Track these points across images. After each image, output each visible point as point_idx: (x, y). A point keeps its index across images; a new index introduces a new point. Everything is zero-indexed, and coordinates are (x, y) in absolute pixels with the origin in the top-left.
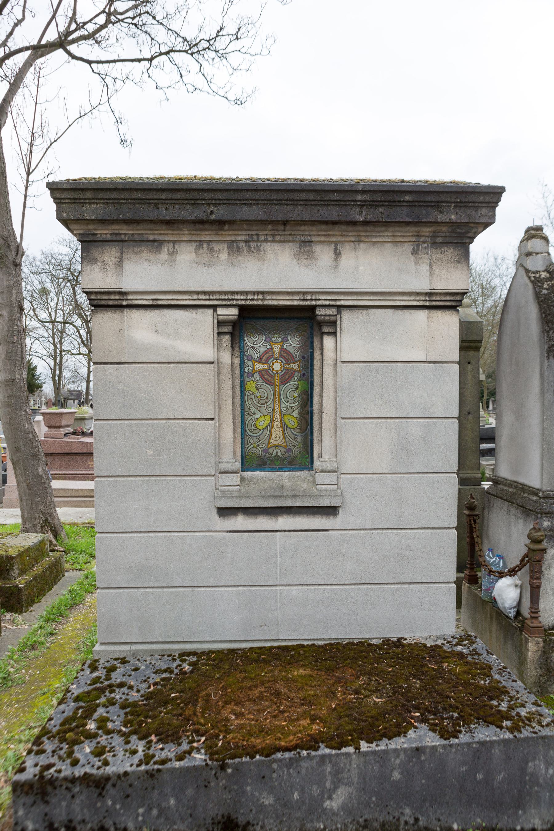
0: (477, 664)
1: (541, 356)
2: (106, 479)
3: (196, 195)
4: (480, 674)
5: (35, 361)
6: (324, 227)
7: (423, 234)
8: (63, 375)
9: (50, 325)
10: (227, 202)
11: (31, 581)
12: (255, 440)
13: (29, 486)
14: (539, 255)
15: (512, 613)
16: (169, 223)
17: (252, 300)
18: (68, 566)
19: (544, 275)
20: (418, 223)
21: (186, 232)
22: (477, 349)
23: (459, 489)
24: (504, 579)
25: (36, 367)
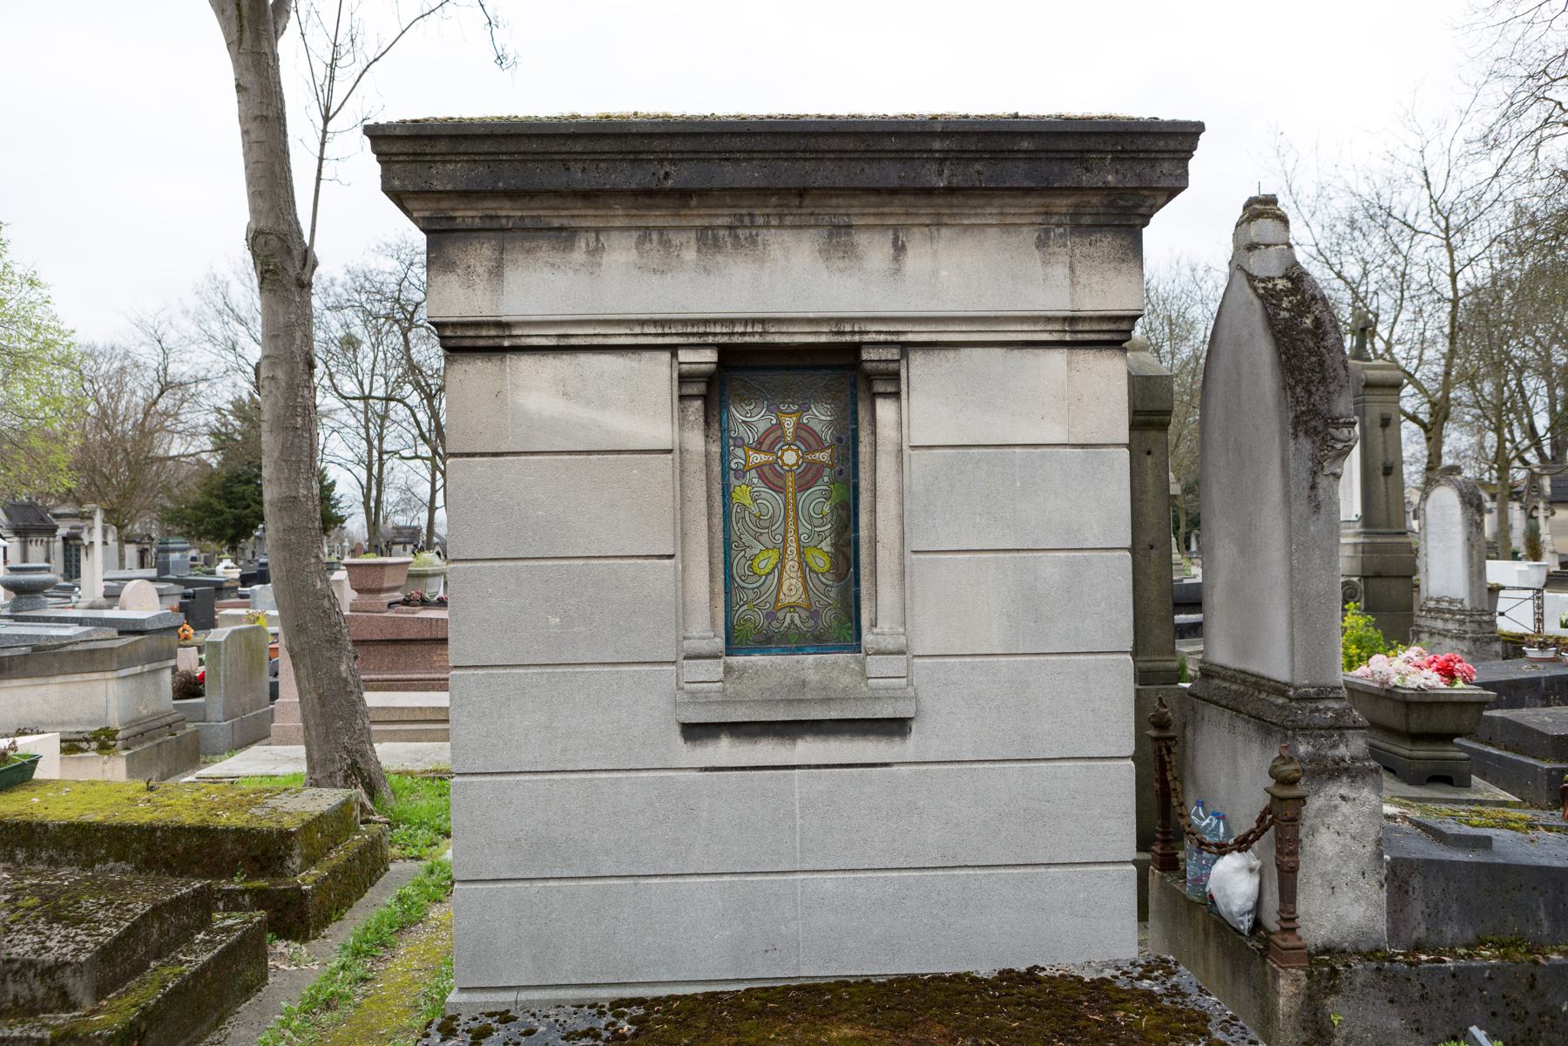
0: (1180, 1012)
1: (1283, 432)
2: (471, 672)
3: (637, 144)
4: (1186, 1030)
5: (332, 473)
6: (873, 199)
7: (1056, 210)
8: (384, 498)
9: (360, 405)
10: (696, 156)
11: (326, 878)
12: (751, 595)
13: (323, 700)
14: (1272, 249)
15: (1245, 924)
16: (589, 196)
17: (743, 334)
18: (395, 851)
19: (1281, 284)
20: (1047, 190)
21: (620, 212)
22: (1164, 426)
23: (1137, 691)
24: (1227, 858)
25: (334, 483)
